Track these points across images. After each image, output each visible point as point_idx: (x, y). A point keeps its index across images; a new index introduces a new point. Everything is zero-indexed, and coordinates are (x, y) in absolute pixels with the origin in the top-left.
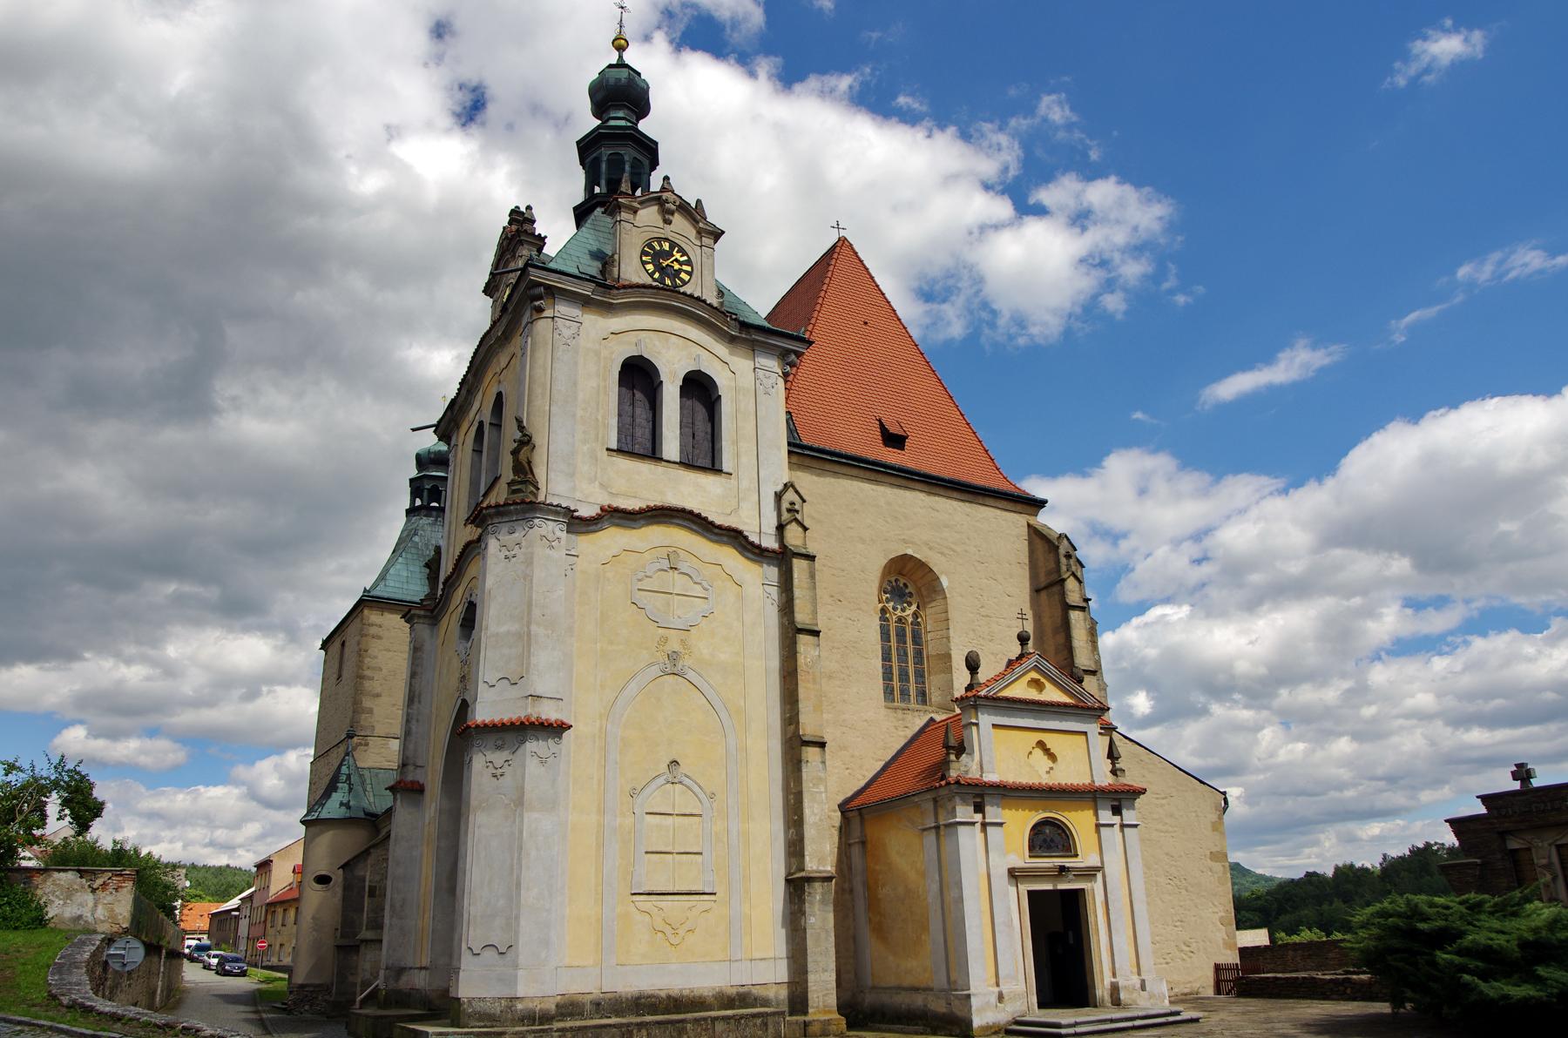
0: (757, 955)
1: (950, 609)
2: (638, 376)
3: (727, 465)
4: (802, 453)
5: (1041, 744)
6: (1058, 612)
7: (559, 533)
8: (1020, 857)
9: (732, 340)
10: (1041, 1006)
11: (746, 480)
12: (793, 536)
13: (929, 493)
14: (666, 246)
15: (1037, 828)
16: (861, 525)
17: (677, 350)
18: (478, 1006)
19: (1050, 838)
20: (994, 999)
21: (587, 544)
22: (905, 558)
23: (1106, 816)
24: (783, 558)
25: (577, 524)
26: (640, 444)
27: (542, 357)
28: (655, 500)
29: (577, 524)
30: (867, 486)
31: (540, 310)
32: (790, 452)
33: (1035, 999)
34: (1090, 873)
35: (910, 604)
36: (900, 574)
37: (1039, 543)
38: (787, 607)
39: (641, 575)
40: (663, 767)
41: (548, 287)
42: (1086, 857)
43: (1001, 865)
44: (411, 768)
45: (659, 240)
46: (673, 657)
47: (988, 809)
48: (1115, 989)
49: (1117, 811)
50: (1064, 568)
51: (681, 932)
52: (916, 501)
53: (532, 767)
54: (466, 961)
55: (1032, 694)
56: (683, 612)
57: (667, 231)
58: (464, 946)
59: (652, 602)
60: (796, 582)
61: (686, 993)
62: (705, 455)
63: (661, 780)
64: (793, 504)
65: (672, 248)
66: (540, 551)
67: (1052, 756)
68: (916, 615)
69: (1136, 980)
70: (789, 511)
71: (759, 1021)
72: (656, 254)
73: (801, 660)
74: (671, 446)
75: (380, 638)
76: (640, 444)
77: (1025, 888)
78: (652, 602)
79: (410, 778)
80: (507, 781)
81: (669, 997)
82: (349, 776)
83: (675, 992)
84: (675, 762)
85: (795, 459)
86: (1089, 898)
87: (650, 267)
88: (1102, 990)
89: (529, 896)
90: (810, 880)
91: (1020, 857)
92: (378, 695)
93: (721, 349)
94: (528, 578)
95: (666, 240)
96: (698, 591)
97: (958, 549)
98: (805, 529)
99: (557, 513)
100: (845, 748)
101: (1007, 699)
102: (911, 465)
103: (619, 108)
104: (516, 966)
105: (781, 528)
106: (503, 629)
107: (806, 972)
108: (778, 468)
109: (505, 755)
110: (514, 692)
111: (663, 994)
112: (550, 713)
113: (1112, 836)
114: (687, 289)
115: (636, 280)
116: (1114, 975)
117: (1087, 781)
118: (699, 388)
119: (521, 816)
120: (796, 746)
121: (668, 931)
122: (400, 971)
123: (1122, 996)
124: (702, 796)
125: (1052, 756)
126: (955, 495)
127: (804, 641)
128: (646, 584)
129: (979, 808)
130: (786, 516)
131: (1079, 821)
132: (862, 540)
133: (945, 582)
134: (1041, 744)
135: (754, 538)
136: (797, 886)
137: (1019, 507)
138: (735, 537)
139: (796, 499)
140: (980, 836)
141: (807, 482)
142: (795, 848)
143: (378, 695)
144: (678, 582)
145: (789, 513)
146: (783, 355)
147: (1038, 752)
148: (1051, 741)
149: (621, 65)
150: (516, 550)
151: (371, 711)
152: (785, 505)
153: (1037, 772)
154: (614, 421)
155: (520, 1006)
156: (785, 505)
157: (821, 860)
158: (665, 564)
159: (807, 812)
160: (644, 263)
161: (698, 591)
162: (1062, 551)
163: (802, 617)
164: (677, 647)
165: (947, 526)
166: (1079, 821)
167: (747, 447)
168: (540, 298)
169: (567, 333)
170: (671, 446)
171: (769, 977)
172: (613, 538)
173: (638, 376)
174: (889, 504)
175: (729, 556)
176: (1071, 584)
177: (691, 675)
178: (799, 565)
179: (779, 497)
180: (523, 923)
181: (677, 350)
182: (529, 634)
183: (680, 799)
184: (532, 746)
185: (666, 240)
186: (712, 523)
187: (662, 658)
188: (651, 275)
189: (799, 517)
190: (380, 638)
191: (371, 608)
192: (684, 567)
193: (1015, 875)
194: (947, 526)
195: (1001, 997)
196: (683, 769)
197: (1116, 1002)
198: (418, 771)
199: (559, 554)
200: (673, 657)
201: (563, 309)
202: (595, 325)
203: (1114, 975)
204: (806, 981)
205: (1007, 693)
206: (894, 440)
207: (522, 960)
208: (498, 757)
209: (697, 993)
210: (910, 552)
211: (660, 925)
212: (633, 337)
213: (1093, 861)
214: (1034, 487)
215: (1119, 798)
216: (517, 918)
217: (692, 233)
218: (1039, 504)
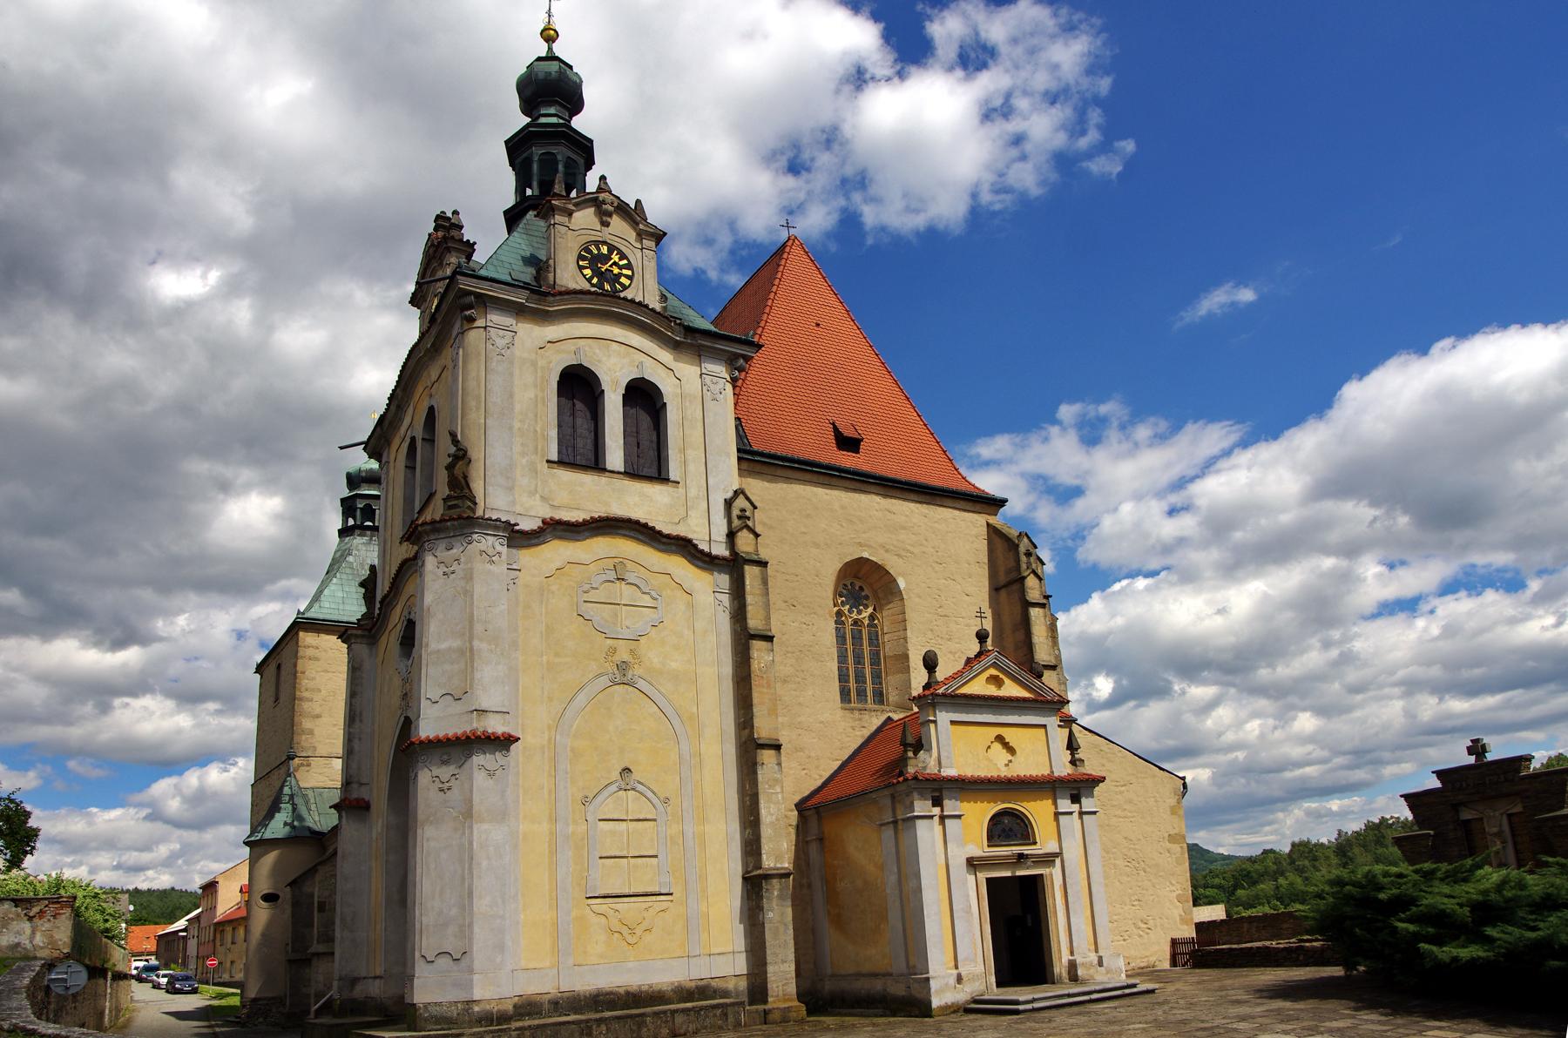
0: (715, 950)
1: (907, 610)
2: (578, 386)
3: (672, 477)
4: (753, 459)
5: (1000, 739)
6: (1018, 609)
7: (499, 548)
8: (978, 846)
9: (676, 346)
10: (999, 985)
11: (695, 488)
12: (744, 542)
13: (885, 496)
14: (605, 250)
15: (996, 819)
16: (814, 530)
17: (618, 357)
18: (434, 1010)
19: (1009, 828)
20: (952, 981)
21: (527, 557)
22: (861, 561)
23: (1065, 805)
24: (734, 565)
25: (518, 538)
26: (582, 452)
27: (475, 369)
28: (599, 511)
29: (518, 538)
30: (820, 491)
31: (471, 320)
32: (739, 459)
33: (993, 979)
34: (1048, 859)
35: (866, 607)
36: (856, 577)
37: (999, 543)
38: (739, 613)
39: (587, 587)
40: (615, 775)
41: (479, 296)
42: (1045, 843)
43: (959, 855)
44: (355, 786)
45: (597, 243)
46: (623, 667)
47: (946, 802)
48: (1072, 966)
49: (1076, 799)
50: (1024, 566)
51: (638, 931)
52: (872, 504)
53: (480, 778)
54: (421, 970)
55: (992, 690)
56: (633, 622)
57: (605, 234)
58: (417, 954)
59: (600, 614)
60: (748, 588)
61: (644, 988)
62: (650, 464)
63: (614, 788)
64: (743, 510)
65: (611, 251)
66: (480, 566)
67: (1011, 750)
68: (872, 617)
69: (1093, 957)
70: (739, 517)
71: (719, 1012)
72: (593, 258)
73: (755, 665)
74: (615, 456)
75: (317, 659)
76: (582, 452)
77: (983, 876)
78: (600, 614)
79: (355, 795)
80: (455, 795)
81: (628, 993)
82: (292, 797)
83: (634, 989)
84: (627, 770)
85: (745, 465)
86: (1047, 883)
87: (588, 272)
88: (1060, 967)
89: (481, 905)
90: (767, 877)
91: (978, 846)
92: (318, 716)
93: (666, 356)
94: (468, 593)
95: (604, 243)
96: (647, 601)
97: (916, 551)
98: (757, 536)
99: (496, 528)
100: (802, 750)
101: (965, 696)
102: (866, 468)
103: (550, 104)
104: (471, 971)
105: (731, 535)
106: (443, 646)
107: (765, 964)
108: (727, 475)
109: (452, 769)
110: (458, 708)
111: (622, 991)
112: (496, 726)
113: (1071, 824)
114: (629, 294)
115: (572, 285)
116: (1072, 953)
117: (1046, 772)
118: (643, 396)
119: (471, 827)
120: (751, 749)
121: (625, 931)
122: (354, 981)
123: (1080, 972)
124: (655, 801)
125: (1011, 750)
126: (912, 496)
127: (757, 645)
128: (592, 596)
129: (937, 802)
130: (736, 523)
131: (1038, 811)
132: (817, 545)
133: (902, 583)
134: (1000, 739)
135: (704, 546)
136: (754, 883)
137: (978, 507)
138: (683, 546)
139: (747, 505)
140: (938, 829)
141: (758, 488)
142: (752, 847)
143: (318, 716)
144: (626, 593)
145: (739, 518)
146: (731, 361)
147: (997, 746)
148: (1008, 734)
149: (551, 57)
150: (455, 566)
151: (311, 732)
152: (735, 512)
153: (996, 764)
154: (554, 433)
155: (476, 1009)
156: (735, 512)
157: (778, 858)
158: (612, 576)
159: (763, 812)
160: (581, 268)
161: (647, 601)
162: (1022, 549)
163: (754, 622)
164: (626, 657)
165: (904, 528)
166: (1038, 811)
167: (695, 455)
168: (471, 307)
169: (500, 343)
170: (615, 456)
171: (727, 970)
172: (557, 552)
173: (578, 386)
174: (843, 507)
175: (678, 565)
176: (1031, 581)
177: (641, 684)
178: (751, 572)
179: (729, 504)
180: (476, 929)
181: (618, 357)
182: (472, 650)
183: (633, 804)
184: (478, 759)
185: (604, 243)
186: (660, 533)
187: (610, 668)
188: (589, 280)
189: (750, 523)
190: (317, 659)
191: (306, 630)
192: (631, 578)
193: (973, 864)
194: (904, 528)
195: (959, 979)
196: (636, 775)
197: (1074, 977)
198: (363, 789)
199: (500, 569)
200: (623, 667)
201: (495, 318)
202: (531, 334)
203: (1072, 953)
204: (766, 972)
205: (966, 690)
206: (849, 443)
207: (477, 965)
208: (445, 772)
209: (656, 988)
210: (866, 555)
211: (616, 926)
212: (571, 346)
213: (1052, 847)
214: (987, 482)
215: (1078, 787)
216: (471, 925)
217: (631, 235)
218: (995, 504)
